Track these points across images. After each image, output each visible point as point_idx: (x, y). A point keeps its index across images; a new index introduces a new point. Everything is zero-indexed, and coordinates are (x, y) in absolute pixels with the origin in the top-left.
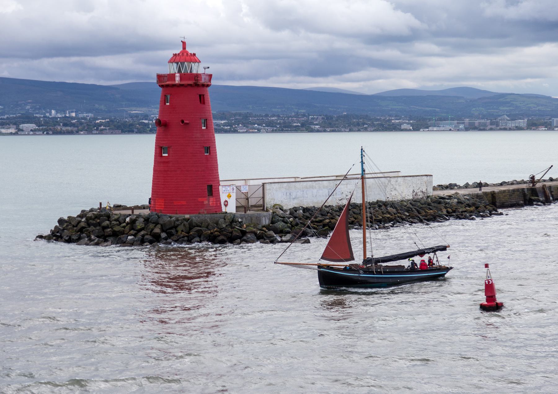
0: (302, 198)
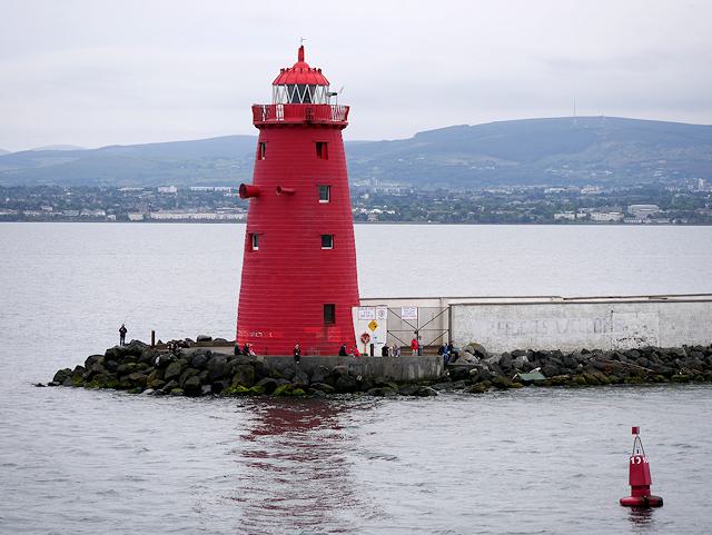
0: (535, 335)
